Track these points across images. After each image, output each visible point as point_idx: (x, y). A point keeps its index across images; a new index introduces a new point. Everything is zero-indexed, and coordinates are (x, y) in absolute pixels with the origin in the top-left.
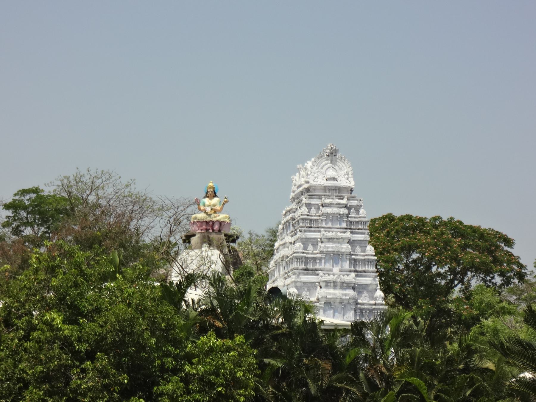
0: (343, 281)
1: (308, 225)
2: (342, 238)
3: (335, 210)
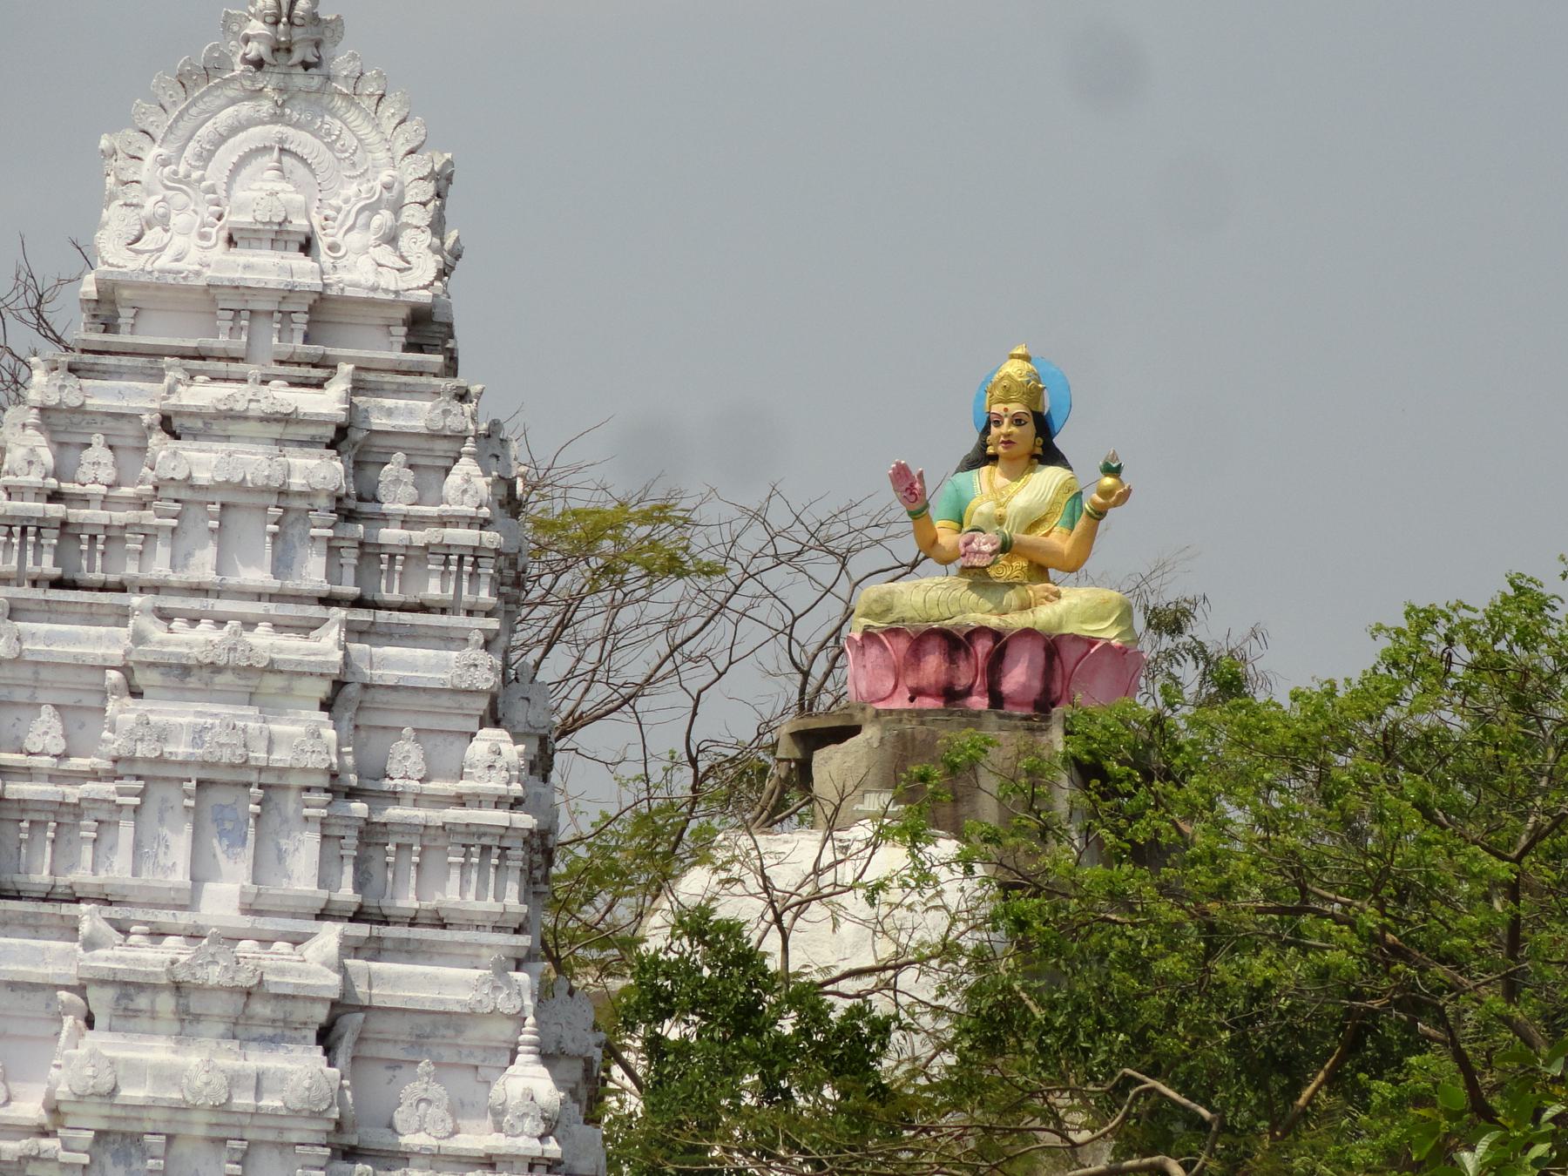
0: (245, 979)
1: (48, 567)
2: (272, 669)
3: (251, 461)
